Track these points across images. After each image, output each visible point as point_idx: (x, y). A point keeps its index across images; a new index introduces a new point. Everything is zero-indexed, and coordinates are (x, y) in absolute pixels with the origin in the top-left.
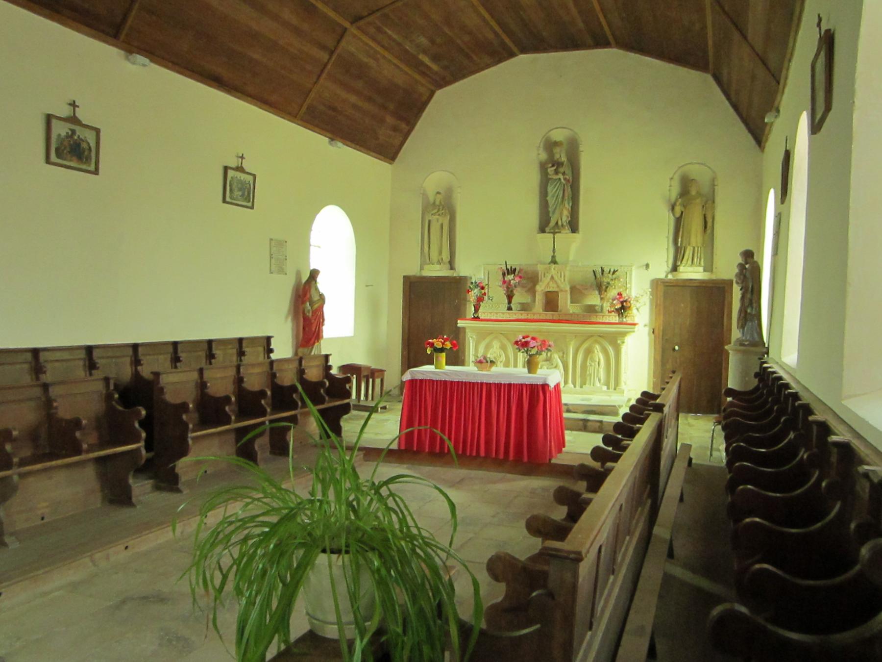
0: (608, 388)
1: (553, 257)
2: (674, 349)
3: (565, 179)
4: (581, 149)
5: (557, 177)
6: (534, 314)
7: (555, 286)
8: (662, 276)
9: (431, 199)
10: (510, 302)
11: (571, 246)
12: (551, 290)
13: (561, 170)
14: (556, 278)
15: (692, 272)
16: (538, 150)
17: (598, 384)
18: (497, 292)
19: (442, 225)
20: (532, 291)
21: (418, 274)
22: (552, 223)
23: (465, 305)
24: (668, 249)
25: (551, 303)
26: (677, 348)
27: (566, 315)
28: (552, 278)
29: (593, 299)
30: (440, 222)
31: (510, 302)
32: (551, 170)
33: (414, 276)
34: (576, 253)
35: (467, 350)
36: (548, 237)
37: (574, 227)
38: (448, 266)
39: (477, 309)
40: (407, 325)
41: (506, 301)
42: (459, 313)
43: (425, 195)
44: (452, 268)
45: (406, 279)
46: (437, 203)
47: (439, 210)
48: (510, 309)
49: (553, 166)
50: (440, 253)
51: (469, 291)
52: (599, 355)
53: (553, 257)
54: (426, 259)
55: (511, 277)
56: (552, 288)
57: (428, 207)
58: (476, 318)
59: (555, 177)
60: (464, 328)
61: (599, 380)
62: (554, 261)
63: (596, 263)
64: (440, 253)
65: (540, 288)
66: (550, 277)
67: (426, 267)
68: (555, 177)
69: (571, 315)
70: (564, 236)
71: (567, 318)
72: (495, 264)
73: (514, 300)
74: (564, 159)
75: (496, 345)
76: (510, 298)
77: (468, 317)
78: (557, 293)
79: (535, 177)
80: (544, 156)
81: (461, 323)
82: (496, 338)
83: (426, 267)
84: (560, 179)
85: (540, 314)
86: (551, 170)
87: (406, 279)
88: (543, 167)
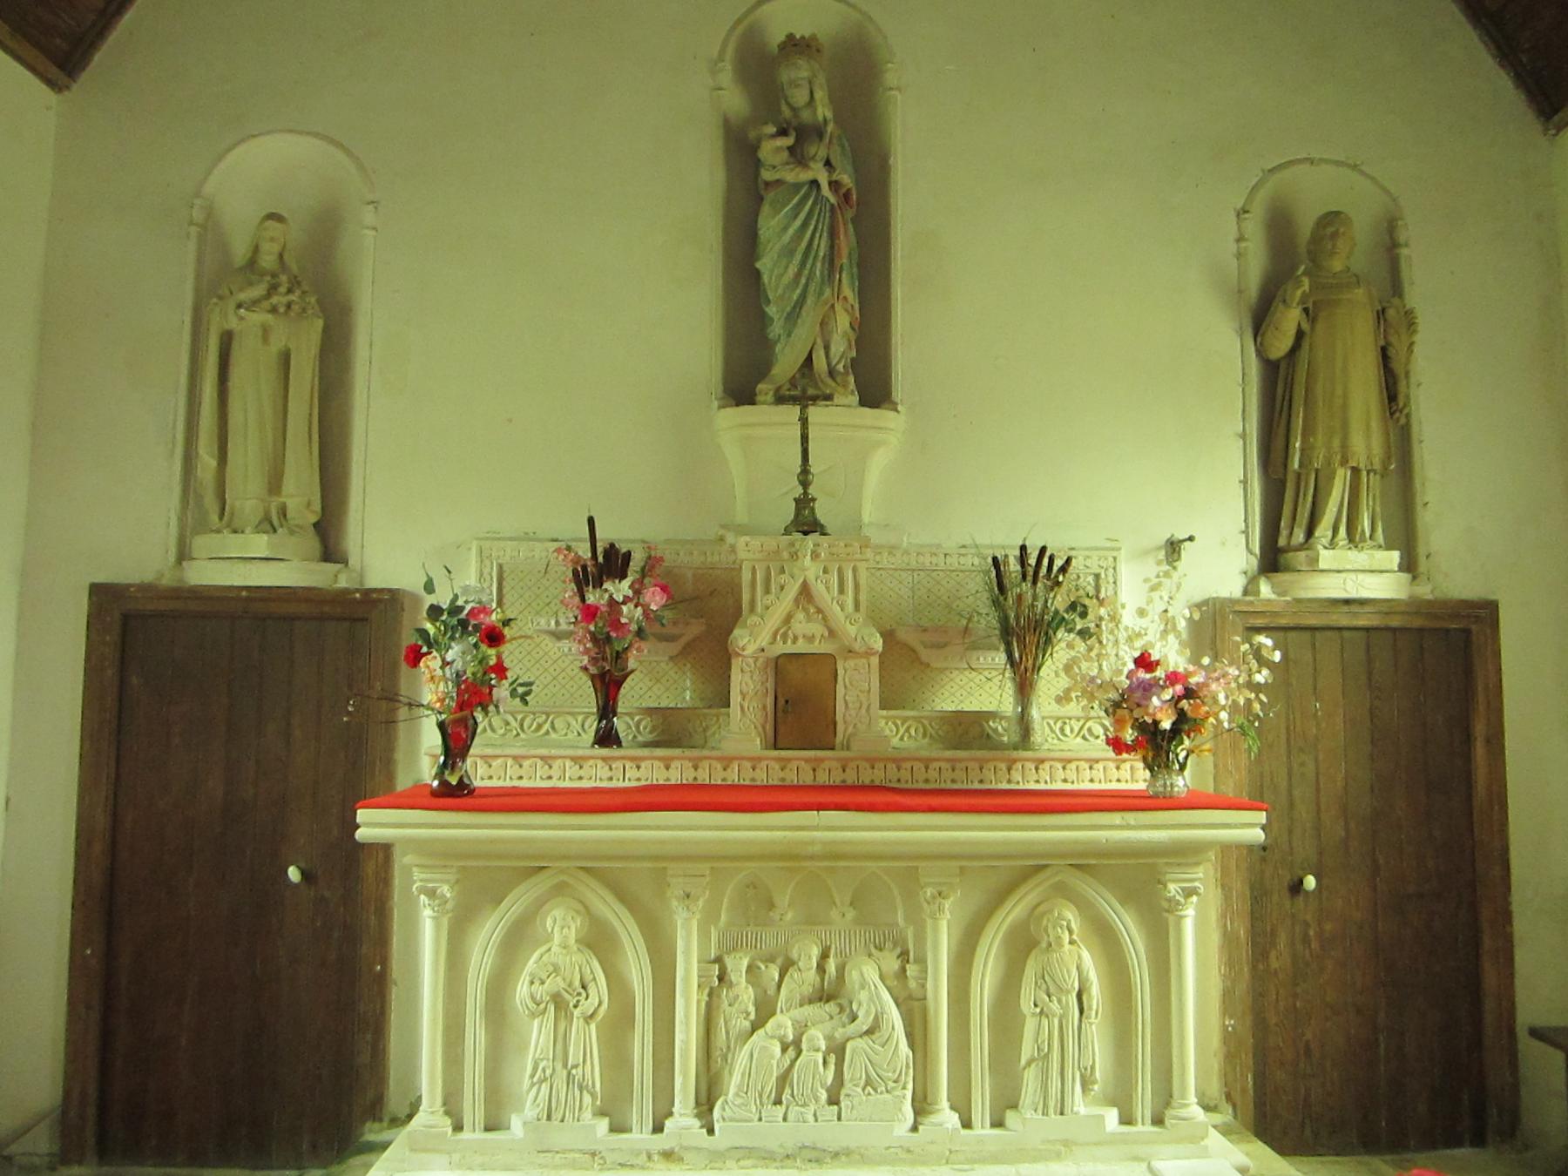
0: (1126, 1120)
1: (804, 502)
2: (1296, 887)
3: (835, 185)
4: (890, 78)
5: (805, 176)
6: (727, 761)
7: (817, 629)
8: (1230, 585)
9: (240, 252)
10: (607, 710)
11: (865, 454)
12: (801, 647)
13: (818, 151)
14: (818, 588)
15: (1355, 573)
16: (714, 72)
17: (1080, 1105)
18: (547, 658)
19: (285, 359)
20: (711, 654)
21: (167, 581)
22: (786, 363)
23: (391, 722)
24: (1245, 482)
25: (800, 709)
26: (1310, 882)
27: (872, 762)
28: (805, 592)
29: (981, 688)
30: (276, 345)
31: (607, 710)
32: (773, 150)
33: (146, 589)
34: (922, 491)
35: (396, 995)
36: (772, 425)
37: (875, 392)
38: (313, 543)
39: (456, 742)
40: (101, 821)
41: (588, 700)
42: (362, 770)
43: (210, 231)
44: (330, 550)
45: (104, 597)
46: (268, 260)
47: (273, 289)
48: (607, 738)
49: (783, 132)
50: (275, 484)
51: (415, 657)
52: (1079, 960)
53: (804, 502)
54: (207, 506)
55: (620, 589)
56: (807, 637)
57: (224, 275)
58: (453, 793)
59: (792, 175)
60: (384, 851)
61: (1086, 1084)
62: (806, 523)
63: (1003, 530)
64: (275, 484)
65: (753, 641)
66: (793, 590)
67: (203, 544)
68: (792, 175)
69: (898, 762)
70: (838, 420)
71: (877, 776)
72: (528, 537)
73: (632, 695)
74: (823, 111)
75: (561, 927)
76: (608, 685)
77: (403, 782)
78: (831, 658)
79: (702, 180)
80: (735, 101)
81: (372, 825)
82: (560, 889)
83: (203, 544)
84: (815, 183)
85: (755, 761)
86: (773, 150)
87: (104, 597)
88: (741, 150)
